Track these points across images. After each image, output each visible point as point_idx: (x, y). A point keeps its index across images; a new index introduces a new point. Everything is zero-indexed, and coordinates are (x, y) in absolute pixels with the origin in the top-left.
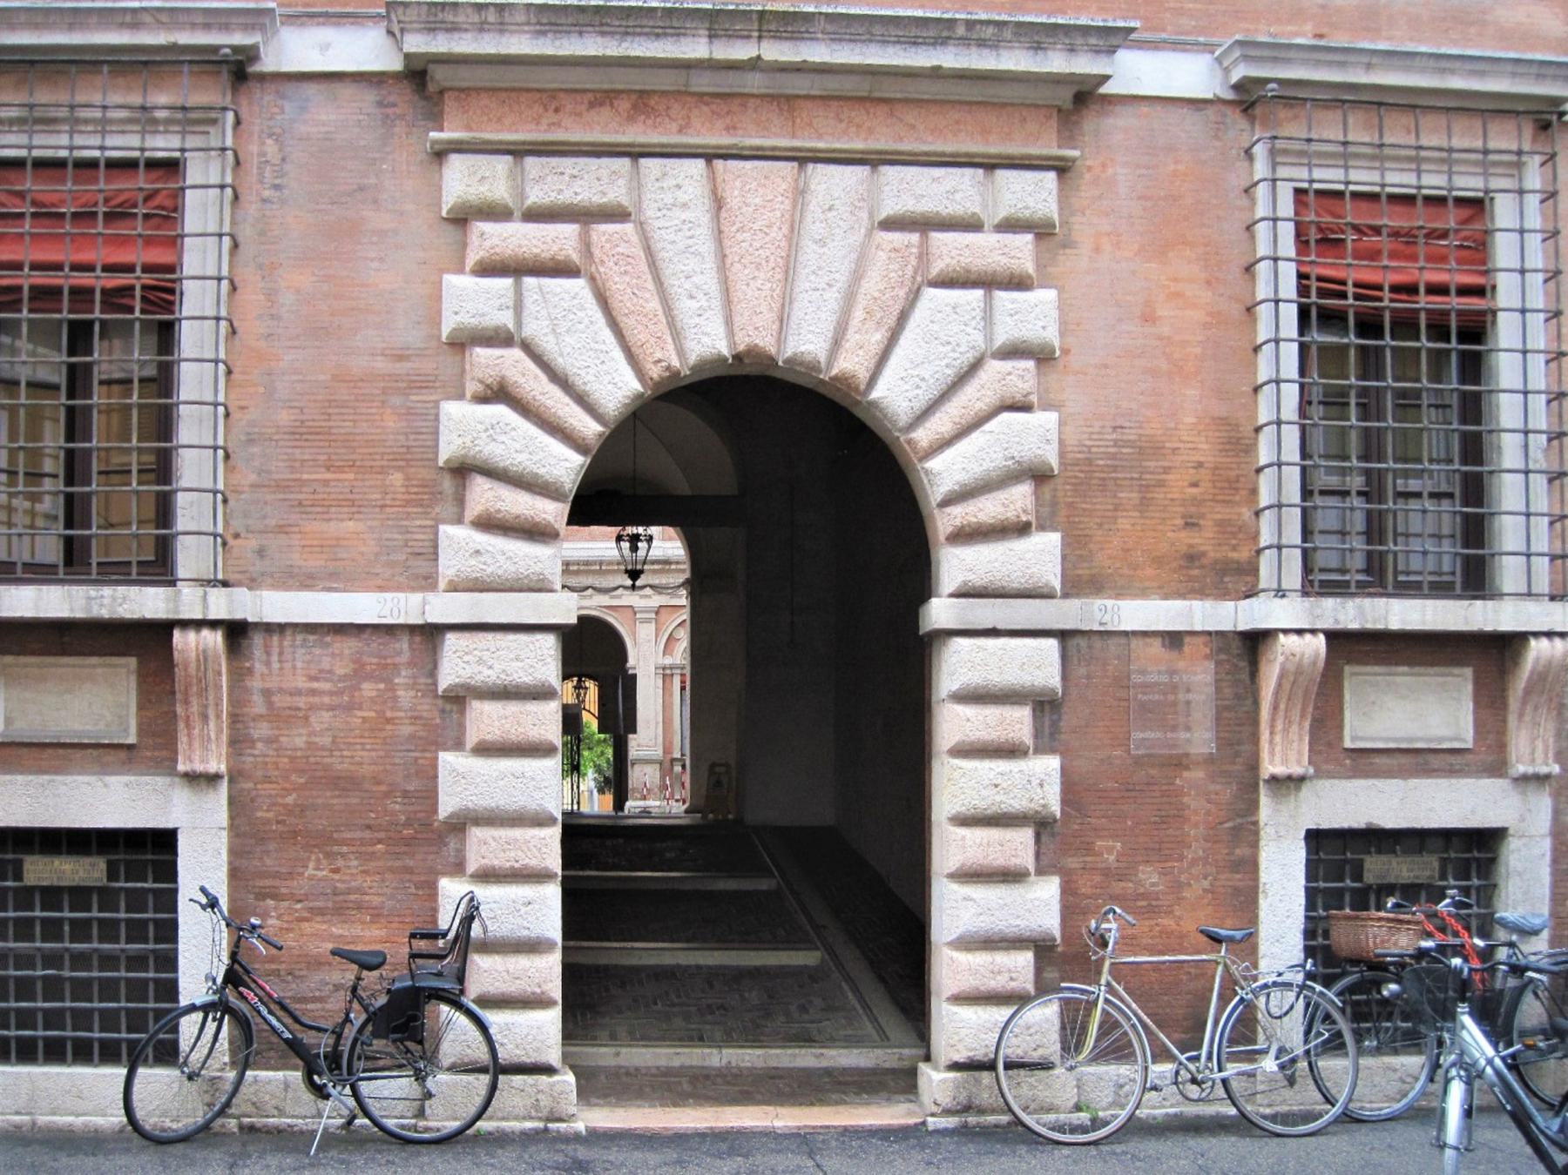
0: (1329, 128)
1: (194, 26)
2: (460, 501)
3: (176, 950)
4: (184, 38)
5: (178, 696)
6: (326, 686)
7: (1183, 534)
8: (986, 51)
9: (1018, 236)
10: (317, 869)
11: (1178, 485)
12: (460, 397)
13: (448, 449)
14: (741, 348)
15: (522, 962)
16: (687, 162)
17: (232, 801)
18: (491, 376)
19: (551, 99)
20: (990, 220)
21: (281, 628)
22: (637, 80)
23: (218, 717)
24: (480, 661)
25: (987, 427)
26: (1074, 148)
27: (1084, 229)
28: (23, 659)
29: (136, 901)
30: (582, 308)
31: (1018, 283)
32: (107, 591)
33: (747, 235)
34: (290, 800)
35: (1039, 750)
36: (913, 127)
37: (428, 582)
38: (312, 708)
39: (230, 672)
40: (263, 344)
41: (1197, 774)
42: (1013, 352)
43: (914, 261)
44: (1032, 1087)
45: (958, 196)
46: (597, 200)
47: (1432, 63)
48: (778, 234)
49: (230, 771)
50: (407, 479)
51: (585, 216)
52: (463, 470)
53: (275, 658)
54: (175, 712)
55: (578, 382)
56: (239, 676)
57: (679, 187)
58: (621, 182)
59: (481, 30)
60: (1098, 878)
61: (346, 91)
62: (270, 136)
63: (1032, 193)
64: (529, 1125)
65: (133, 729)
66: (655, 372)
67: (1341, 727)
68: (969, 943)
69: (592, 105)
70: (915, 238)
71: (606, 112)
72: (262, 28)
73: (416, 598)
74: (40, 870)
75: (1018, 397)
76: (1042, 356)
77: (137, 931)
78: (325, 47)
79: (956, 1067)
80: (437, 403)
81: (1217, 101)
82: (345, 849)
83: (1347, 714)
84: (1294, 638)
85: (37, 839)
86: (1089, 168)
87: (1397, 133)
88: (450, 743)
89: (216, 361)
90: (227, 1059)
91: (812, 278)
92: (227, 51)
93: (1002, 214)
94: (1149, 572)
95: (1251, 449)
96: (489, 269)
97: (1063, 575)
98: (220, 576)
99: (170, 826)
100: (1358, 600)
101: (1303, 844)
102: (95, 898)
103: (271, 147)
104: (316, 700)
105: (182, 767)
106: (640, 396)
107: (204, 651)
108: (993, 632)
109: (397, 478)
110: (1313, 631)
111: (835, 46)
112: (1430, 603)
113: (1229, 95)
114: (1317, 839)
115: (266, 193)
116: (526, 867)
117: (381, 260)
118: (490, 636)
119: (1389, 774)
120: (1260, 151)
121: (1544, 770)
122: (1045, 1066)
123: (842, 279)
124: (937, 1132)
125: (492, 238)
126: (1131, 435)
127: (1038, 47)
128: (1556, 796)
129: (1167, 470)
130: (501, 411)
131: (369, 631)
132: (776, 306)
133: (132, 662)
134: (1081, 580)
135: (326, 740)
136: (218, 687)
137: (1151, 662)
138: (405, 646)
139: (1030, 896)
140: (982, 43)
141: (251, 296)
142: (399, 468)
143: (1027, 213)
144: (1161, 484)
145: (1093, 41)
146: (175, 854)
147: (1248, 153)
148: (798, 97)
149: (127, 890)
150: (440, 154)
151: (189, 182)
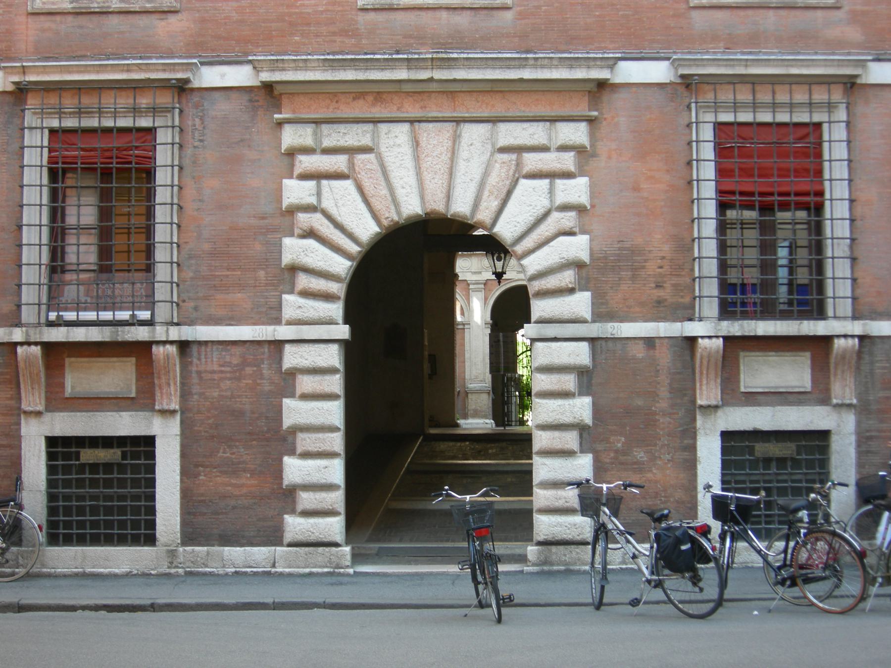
0: (726, 95)
1: (157, 70)
2: (293, 284)
3: (155, 492)
5: (155, 375)
6: (228, 369)
7: (655, 291)
8: (545, 70)
9: (567, 154)
10: (224, 453)
12: (292, 235)
13: (287, 258)
14: (428, 210)
15: (323, 495)
16: (400, 124)
17: (182, 422)
18: (305, 226)
20: (554, 146)
21: (206, 343)
22: (376, 88)
23: (175, 384)
25: (552, 244)
26: (596, 110)
27: (603, 148)
29: (136, 469)
30: (349, 195)
33: (430, 159)
34: (210, 421)
35: (581, 394)
36: (515, 103)
37: (277, 321)
38: (222, 379)
39: (181, 363)
40: (195, 213)
43: (513, 168)
44: (578, 553)
45: (536, 136)
46: (356, 144)
47: (780, 63)
48: (446, 157)
49: (181, 408)
50: (267, 273)
52: (294, 269)
53: (203, 357)
54: (154, 383)
55: (349, 228)
56: (185, 366)
57: (396, 137)
58: (368, 135)
59: (296, 70)
60: (612, 455)
61: (234, 95)
62: (197, 117)
63: (577, 133)
64: (326, 570)
66: (386, 223)
67: (738, 382)
69: (354, 99)
70: (514, 156)
71: (361, 102)
73: (270, 328)
74: (88, 456)
75: (567, 229)
76: (580, 209)
77: (136, 483)
79: (539, 543)
81: (671, 84)
82: (237, 444)
83: (742, 376)
84: (707, 341)
85: (100, 441)
86: (605, 119)
90: (179, 541)
91: (463, 177)
92: (174, 81)
94: (637, 309)
96: (305, 177)
98: (175, 320)
99: (152, 434)
100: (740, 322)
101: (719, 438)
102: (115, 468)
104: (223, 375)
105: (157, 407)
106: (378, 234)
107: (167, 355)
109: (262, 274)
110: (717, 337)
111: (470, 71)
112: (779, 322)
114: (726, 436)
115: (196, 144)
116: (325, 451)
117: (252, 173)
118: (306, 345)
119: (767, 404)
121: (848, 402)
123: (477, 177)
125: (305, 162)
126: (627, 245)
127: (571, 67)
129: (646, 261)
130: (311, 243)
131: (247, 345)
133: (133, 360)
134: (601, 314)
137: (639, 351)
138: (266, 350)
139: (575, 463)
140: (543, 67)
141: (190, 192)
142: (263, 269)
143: (571, 143)
144: (644, 267)
145: (598, 63)
146: (155, 447)
147: (689, 107)
148: (457, 92)
149: (131, 464)
150: (280, 124)
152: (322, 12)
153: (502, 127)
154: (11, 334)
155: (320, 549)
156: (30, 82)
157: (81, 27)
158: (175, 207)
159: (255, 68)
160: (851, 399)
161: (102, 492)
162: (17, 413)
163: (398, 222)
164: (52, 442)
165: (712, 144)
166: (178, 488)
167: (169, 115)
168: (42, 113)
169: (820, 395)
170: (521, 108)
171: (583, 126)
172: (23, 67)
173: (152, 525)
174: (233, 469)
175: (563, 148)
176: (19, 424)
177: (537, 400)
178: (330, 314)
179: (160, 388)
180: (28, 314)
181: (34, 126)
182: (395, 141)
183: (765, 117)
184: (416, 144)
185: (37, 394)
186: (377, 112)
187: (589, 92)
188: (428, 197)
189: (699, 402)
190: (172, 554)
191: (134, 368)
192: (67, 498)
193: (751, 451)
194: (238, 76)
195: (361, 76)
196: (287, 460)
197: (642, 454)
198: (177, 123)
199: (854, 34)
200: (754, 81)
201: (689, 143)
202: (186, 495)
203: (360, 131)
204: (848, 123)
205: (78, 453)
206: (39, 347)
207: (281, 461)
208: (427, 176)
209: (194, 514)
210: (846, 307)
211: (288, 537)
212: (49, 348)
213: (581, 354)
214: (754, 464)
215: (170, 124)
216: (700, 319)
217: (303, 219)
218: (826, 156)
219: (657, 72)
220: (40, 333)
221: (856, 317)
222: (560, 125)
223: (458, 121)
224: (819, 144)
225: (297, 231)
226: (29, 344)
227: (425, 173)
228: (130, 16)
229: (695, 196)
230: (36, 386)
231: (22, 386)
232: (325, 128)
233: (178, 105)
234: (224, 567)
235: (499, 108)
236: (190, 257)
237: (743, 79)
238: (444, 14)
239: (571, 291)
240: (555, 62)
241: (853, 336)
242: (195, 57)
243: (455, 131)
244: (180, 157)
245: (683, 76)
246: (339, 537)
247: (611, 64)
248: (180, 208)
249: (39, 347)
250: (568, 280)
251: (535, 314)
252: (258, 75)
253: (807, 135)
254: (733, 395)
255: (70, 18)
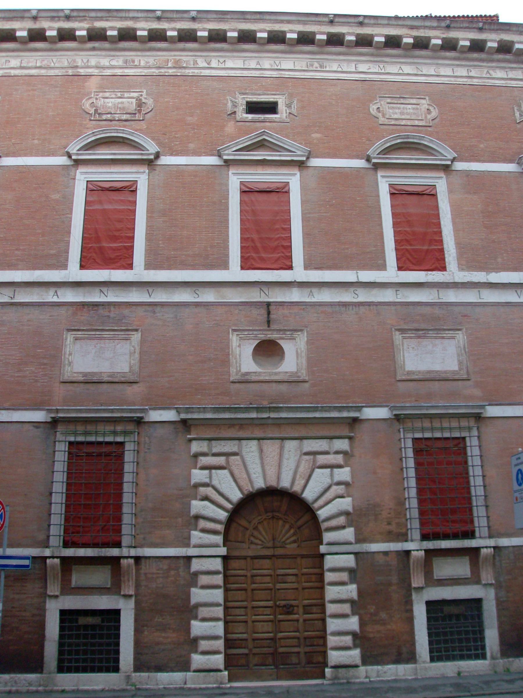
0: (418, 424)
1: (127, 412)
3: (119, 641)
4: (125, 415)
5: (122, 575)
6: (161, 572)
11: (385, 514)
13: (193, 512)
14: (268, 486)
17: (136, 602)
18: (203, 494)
19: (218, 426)
21: (149, 557)
23: (132, 579)
24: (201, 565)
25: (333, 502)
26: (353, 433)
28: (81, 566)
29: (109, 628)
30: (227, 477)
31: (340, 466)
32: (103, 550)
35: (351, 583)
37: (188, 545)
38: (158, 577)
41: (394, 588)
42: (339, 483)
43: (312, 463)
45: (323, 447)
46: (230, 451)
48: (277, 458)
51: (227, 455)
52: (197, 517)
53: (148, 565)
56: (137, 570)
58: (236, 447)
61: (166, 425)
62: (147, 436)
63: (343, 445)
64: (215, 686)
65: (109, 583)
66: (246, 492)
67: (433, 573)
68: (334, 634)
69: (229, 428)
72: (145, 412)
74: (83, 621)
76: (346, 484)
77: (109, 636)
78: (161, 415)
79: (332, 667)
80: (190, 501)
81: (390, 419)
83: (435, 571)
84: (416, 552)
87: (437, 424)
88: (84, 254)
89: (132, 493)
90: (132, 670)
93: (335, 450)
95: (404, 504)
96: (203, 468)
97: (355, 539)
99: (119, 608)
101: (425, 605)
103: (147, 439)
104: (158, 575)
105: (122, 593)
108: (336, 554)
109: (180, 520)
113: (393, 417)
115: (146, 450)
120: (401, 430)
121: (490, 582)
122: (356, 666)
124: (326, 685)
125: (204, 460)
128: (496, 589)
129: (381, 511)
130: (206, 503)
132: (276, 475)
133: (109, 567)
134: (360, 540)
135: (161, 585)
136: (133, 573)
137: (381, 559)
140: (326, 411)
143: (341, 449)
144: (380, 514)
147: (399, 431)
150: (190, 440)
151: (126, 449)
152: (212, 383)
153: (305, 442)
154: (43, 552)
155: (212, 674)
156: (60, 417)
157: (88, 389)
158: (134, 484)
159: (177, 411)
160: (491, 581)
161: (90, 642)
162: (44, 596)
163: (252, 492)
164: (63, 612)
165: (412, 449)
166: (133, 639)
167: (132, 435)
168: (66, 434)
169: (475, 579)
170: (314, 431)
171: (346, 441)
172: (57, 409)
173: (117, 660)
174: (164, 628)
175: (337, 452)
176: (45, 602)
177: (329, 587)
178: (216, 542)
179: (124, 582)
180: (54, 541)
181: (61, 440)
182: (250, 450)
183: (438, 435)
184: (261, 451)
185: (56, 585)
186: (241, 434)
187: (349, 423)
188: (268, 478)
189: (414, 585)
190: (128, 677)
191: (110, 571)
192: (70, 645)
193: (442, 611)
194: (170, 415)
195: (232, 416)
196: (193, 623)
197: (385, 615)
198: (136, 440)
199: (477, 392)
200: (431, 417)
201: (401, 449)
202: (137, 643)
203: (232, 444)
204: (479, 437)
205: (77, 619)
206: (59, 560)
207: (189, 624)
208: (267, 468)
209: (141, 654)
210: (485, 532)
211: (194, 666)
212: (64, 560)
213: (349, 561)
214: (443, 619)
215: (132, 440)
216: (412, 541)
217: (202, 490)
218: (469, 454)
219: (381, 413)
220: (60, 551)
221: (490, 536)
222: (335, 441)
223: (283, 439)
224: (465, 448)
225: (199, 497)
226: (53, 557)
227: (266, 466)
228: (113, 384)
229: (405, 476)
230: (56, 581)
231: (48, 581)
232: (214, 442)
233: (137, 430)
234: (157, 684)
235: (303, 432)
236: (142, 511)
237: (426, 416)
238: (274, 384)
239: (344, 527)
240: (332, 409)
241: (490, 547)
242: (146, 406)
243: (281, 444)
244: (137, 458)
245: (395, 415)
246: (222, 667)
247: (359, 409)
248: (137, 484)
249: (59, 560)
250: (342, 522)
251: (325, 541)
252: (179, 415)
253: (459, 443)
254: (431, 582)
255: (82, 385)
